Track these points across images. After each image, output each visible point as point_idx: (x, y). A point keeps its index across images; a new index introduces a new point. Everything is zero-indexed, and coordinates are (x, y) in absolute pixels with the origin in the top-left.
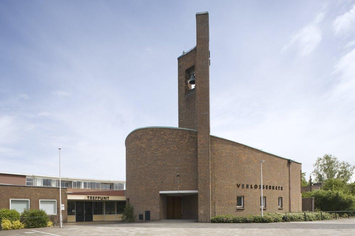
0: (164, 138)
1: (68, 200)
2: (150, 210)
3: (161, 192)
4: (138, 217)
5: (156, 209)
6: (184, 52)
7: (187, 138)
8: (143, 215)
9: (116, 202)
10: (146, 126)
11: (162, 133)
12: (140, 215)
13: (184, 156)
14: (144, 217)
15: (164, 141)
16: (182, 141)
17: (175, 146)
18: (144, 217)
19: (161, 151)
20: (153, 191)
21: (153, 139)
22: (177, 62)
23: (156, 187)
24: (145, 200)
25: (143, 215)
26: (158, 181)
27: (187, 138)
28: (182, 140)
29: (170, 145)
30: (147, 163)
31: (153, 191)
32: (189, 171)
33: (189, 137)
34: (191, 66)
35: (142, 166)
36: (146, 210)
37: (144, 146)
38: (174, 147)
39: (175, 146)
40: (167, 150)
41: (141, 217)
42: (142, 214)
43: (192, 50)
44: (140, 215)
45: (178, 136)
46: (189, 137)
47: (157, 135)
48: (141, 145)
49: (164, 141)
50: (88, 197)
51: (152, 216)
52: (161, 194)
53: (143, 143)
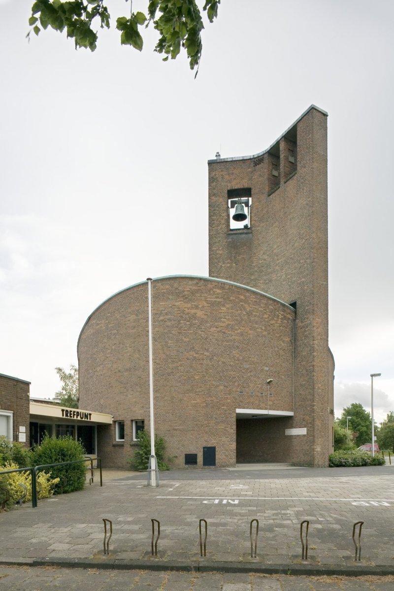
0: (245, 309)
1: (237, 414)
2: (215, 445)
3: (239, 411)
4: (182, 460)
5: (227, 445)
6: (218, 155)
7: (280, 317)
8: (196, 455)
9: (76, 428)
10: (175, 274)
11: (242, 297)
12: (186, 455)
13: (276, 349)
14: (200, 459)
15: (244, 313)
16: (273, 322)
17: (264, 328)
18: (200, 459)
19: (239, 331)
20: (223, 407)
21: (224, 306)
22: (206, 167)
23: (229, 401)
24: (202, 426)
25: (196, 455)
26: (234, 389)
27: (280, 317)
28: (273, 319)
29: (256, 323)
30: (208, 350)
31: (223, 407)
32: (283, 377)
33: (283, 317)
34: (242, 187)
35: (195, 355)
36: (205, 445)
37: (200, 313)
38: (261, 329)
39: (264, 328)
40: (250, 332)
41: (191, 459)
42: (194, 452)
43: (246, 160)
44: (186, 455)
45: (267, 310)
46: (283, 317)
47: (231, 298)
48: (193, 311)
49: (244, 313)
50: (63, 410)
51: (219, 456)
52: (238, 415)
53: (197, 307)
